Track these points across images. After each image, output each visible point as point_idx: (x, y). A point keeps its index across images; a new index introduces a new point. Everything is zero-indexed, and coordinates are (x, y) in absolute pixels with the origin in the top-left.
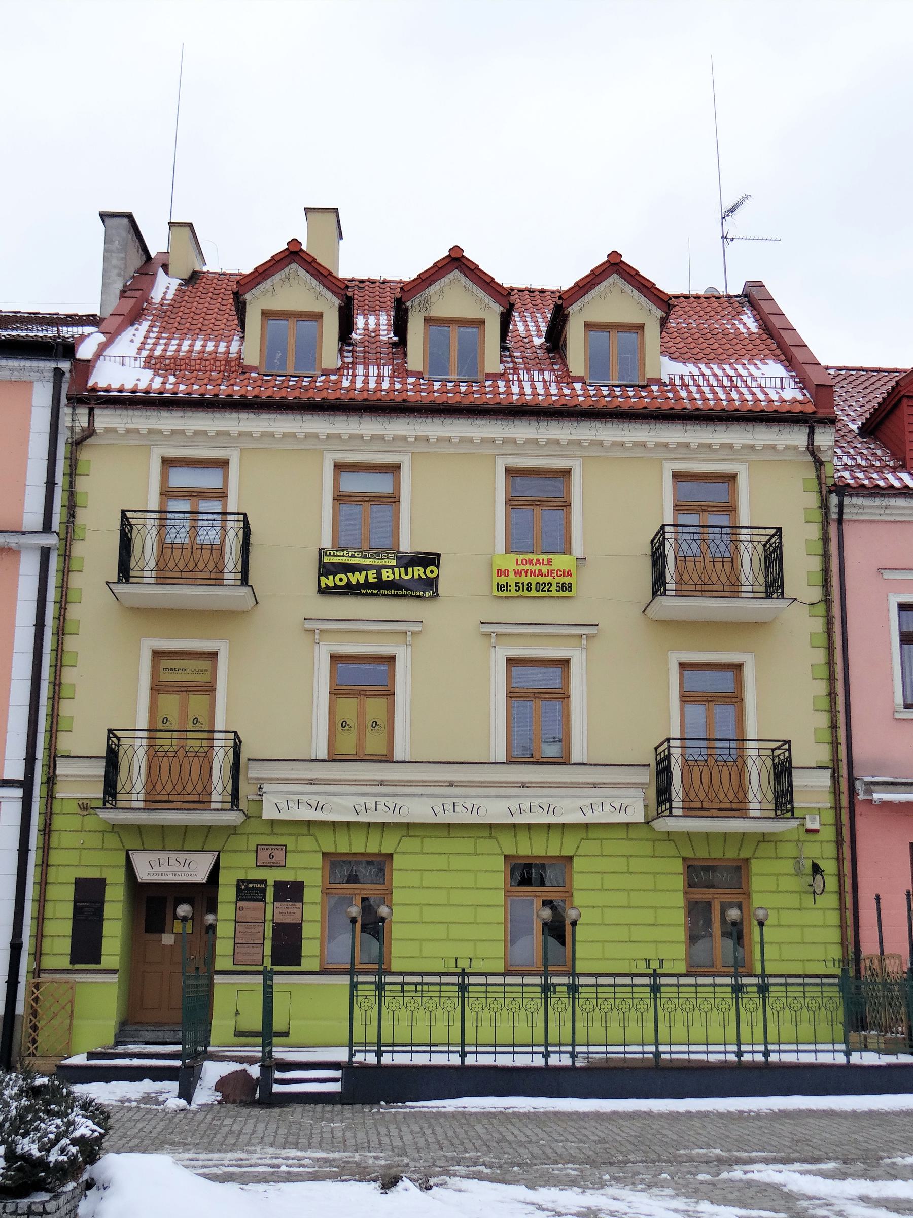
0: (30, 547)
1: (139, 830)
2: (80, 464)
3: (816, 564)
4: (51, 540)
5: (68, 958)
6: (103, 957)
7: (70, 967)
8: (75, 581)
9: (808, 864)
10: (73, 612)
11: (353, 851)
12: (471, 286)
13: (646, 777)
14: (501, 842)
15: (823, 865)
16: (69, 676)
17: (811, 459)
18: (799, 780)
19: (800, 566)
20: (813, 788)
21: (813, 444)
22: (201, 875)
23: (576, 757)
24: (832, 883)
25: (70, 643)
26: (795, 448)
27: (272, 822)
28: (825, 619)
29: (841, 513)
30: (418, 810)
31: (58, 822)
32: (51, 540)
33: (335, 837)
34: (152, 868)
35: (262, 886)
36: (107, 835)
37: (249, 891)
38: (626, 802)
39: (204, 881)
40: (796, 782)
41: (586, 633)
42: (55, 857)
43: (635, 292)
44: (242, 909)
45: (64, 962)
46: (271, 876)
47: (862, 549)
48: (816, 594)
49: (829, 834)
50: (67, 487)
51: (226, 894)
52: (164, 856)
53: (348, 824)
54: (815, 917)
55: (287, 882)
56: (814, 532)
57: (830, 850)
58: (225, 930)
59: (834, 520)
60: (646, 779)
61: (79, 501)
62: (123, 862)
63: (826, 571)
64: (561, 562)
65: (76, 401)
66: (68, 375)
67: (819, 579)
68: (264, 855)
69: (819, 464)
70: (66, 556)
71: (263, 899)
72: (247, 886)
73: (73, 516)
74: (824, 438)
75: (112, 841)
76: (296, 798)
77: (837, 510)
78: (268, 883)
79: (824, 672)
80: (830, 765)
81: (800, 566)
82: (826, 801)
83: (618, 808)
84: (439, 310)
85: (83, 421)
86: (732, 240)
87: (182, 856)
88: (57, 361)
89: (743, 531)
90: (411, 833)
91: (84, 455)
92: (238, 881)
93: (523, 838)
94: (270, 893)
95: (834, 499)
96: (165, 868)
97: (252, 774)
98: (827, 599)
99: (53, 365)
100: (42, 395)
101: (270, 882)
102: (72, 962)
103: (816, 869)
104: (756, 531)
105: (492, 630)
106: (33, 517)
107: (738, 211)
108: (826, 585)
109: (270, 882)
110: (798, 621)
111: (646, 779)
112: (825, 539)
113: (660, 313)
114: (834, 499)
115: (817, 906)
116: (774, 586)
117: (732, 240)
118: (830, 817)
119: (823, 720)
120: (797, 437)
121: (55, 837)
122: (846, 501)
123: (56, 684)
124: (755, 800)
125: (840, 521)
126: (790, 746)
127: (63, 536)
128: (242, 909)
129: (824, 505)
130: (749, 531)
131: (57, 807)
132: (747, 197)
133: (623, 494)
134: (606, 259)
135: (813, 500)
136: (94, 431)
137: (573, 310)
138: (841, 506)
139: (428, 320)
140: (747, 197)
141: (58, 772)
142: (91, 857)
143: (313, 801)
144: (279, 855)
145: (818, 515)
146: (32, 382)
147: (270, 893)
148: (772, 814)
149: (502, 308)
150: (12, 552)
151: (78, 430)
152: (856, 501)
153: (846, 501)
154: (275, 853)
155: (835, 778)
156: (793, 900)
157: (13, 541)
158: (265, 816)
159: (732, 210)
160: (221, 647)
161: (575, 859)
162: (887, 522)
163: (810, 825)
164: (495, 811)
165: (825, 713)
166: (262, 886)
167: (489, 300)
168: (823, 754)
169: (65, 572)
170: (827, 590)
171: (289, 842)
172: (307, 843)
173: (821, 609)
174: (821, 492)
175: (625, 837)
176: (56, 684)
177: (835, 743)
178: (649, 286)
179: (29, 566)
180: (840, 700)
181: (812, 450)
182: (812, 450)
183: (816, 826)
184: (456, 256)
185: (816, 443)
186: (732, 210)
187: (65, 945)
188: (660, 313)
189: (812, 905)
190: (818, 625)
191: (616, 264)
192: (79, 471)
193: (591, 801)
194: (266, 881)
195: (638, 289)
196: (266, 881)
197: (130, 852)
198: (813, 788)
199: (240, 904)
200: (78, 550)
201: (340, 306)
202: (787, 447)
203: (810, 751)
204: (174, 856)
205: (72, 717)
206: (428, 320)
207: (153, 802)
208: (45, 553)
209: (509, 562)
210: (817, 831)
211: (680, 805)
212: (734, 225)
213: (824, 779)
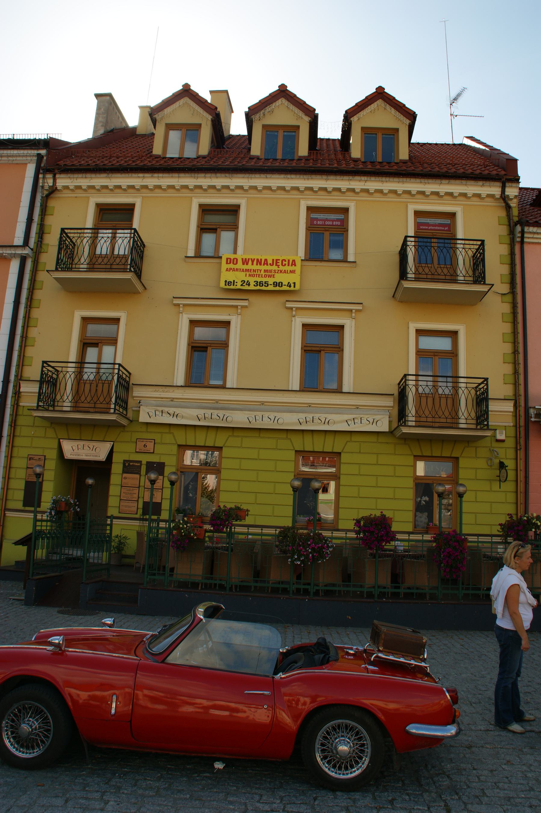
0: (14, 256)
2: (48, 209)
3: (505, 270)
4: (26, 251)
5: (21, 503)
6: (42, 503)
7: (23, 508)
9: (497, 461)
11: (188, 444)
12: (292, 107)
13: (389, 402)
15: (506, 462)
16: (33, 332)
17: (504, 204)
18: (493, 406)
20: (501, 411)
21: (504, 194)
22: (102, 456)
24: (511, 475)
25: (35, 313)
26: (492, 196)
27: (147, 424)
28: (512, 305)
29: (522, 237)
30: (239, 419)
31: (21, 421)
32: (26, 251)
33: (186, 434)
34: (73, 450)
35: (139, 464)
36: (48, 429)
37: (130, 467)
38: (377, 417)
39: (104, 460)
40: (491, 408)
42: (18, 442)
43: (393, 109)
44: (125, 478)
45: (19, 505)
46: (145, 459)
48: (505, 288)
49: (511, 443)
50: (40, 222)
51: (117, 468)
52: (81, 443)
53: (195, 426)
55: (154, 463)
56: (504, 250)
57: (511, 453)
58: (114, 490)
59: (518, 242)
60: (391, 404)
61: (46, 230)
62: (56, 446)
63: (513, 274)
66: (45, 158)
67: (507, 279)
68: (140, 445)
71: (139, 473)
72: (129, 464)
73: (42, 238)
76: (161, 409)
77: (519, 235)
78: (143, 463)
79: (510, 338)
80: (513, 398)
82: (510, 422)
83: (371, 422)
85: (50, 182)
86: (456, 116)
87: (91, 444)
88: (38, 149)
89: (459, 242)
90: (235, 434)
91: (51, 203)
92: (124, 460)
93: (308, 438)
94: (143, 469)
96: (81, 451)
97: (135, 394)
98: (513, 292)
99: (36, 152)
100: (31, 169)
101: (144, 462)
102: (25, 505)
103: (502, 465)
104: (467, 242)
106: (19, 240)
107: (460, 100)
109: (144, 462)
111: (391, 404)
112: (512, 254)
113: (408, 122)
114: (519, 228)
115: (502, 489)
117: (456, 116)
118: (512, 432)
121: (18, 429)
122: (526, 229)
123: (24, 337)
124: (463, 417)
125: (522, 242)
126: (487, 382)
127: (35, 250)
128: (125, 478)
129: (512, 232)
130: (463, 242)
131: (20, 411)
132: (464, 89)
134: (375, 91)
135: (504, 230)
136: (56, 188)
137: (354, 119)
138: (523, 232)
140: (464, 89)
141: (21, 390)
143: (171, 410)
144: (150, 446)
145: (507, 240)
146: (27, 164)
147: (143, 469)
148: (474, 426)
149: (310, 119)
150: (7, 259)
151: (46, 188)
152: (531, 229)
153: (526, 229)
154: (148, 444)
155: (516, 406)
158: (141, 419)
159: (455, 99)
160: (123, 315)
161: (342, 454)
163: (499, 437)
164: (289, 420)
165: (511, 364)
166: (139, 464)
167: (301, 114)
168: (508, 390)
170: (513, 285)
171: (157, 437)
172: (168, 438)
173: (509, 298)
174: (510, 225)
175: (376, 441)
176: (24, 337)
177: (516, 384)
178: (402, 106)
179: (14, 266)
181: (504, 198)
183: (503, 437)
184: (283, 89)
185: (506, 193)
186: (455, 99)
187: (20, 495)
188: (408, 122)
189: (499, 489)
190: (507, 308)
191: (381, 93)
192: (47, 213)
193: (354, 416)
194: (141, 461)
195: (395, 108)
196: (141, 461)
197: (61, 440)
198: (501, 411)
199: (125, 475)
201: (212, 121)
202: (489, 196)
203: (500, 388)
204: (86, 443)
205: (32, 357)
207: (76, 408)
208: (23, 260)
210: (503, 441)
211: (414, 419)
212: (458, 108)
213: (509, 407)
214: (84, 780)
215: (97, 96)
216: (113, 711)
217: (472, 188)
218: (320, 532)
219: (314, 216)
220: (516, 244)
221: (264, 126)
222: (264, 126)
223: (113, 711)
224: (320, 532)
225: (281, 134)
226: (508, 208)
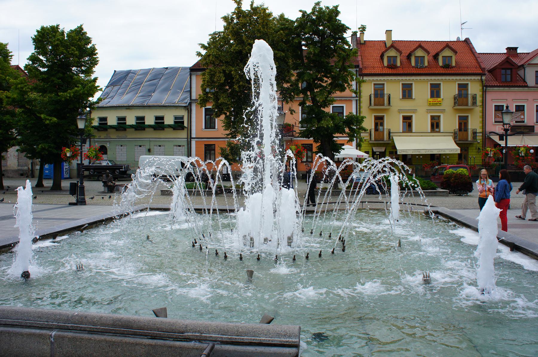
1: (374, 143)
3: (481, 99)
4: (358, 99)
8: (361, 105)
10: (362, 110)
14: (474, 62)
19: (479, 99)
23: (442, 130)
41: (443, 111)
47: (489, 96)
48: (481, 104)
49: (481, 143)
54: (478, 156)
56: (481, 93)
57: (481, 145)
64: (439, 99)
65: (360, 75)
69: (482, 82)
70: (360, 100)
74: (484, 78)
75: (370, 145)
81: (479, 99)
84: (417, 55)
95: (485, 88)
103: (479, 149)
105: (428, 111)
108: (483, 102)
110: (478, 109)
112: (483, 94)
114: (485, 88)
116: (474, 103)
118: (481, 140)
119: (481, 125)
120: (479, 78)
129: (483, 89)
133: (449, 89)
135: (481, 88)
139: (415, 57)
142: (366, 148)
156: (475, 153)
157: (352, 99)
162: (22, 326)
168: (481, 130)
169: (360, 103)
177: (483, 128)
180: (343, 99)
181: (481, 79)
182: (481, 79)
190: (481, 109)
200: (361, 99)
203: (479, 130)
206: (415, 57)
208: (357, 100)
209: (431, 100)
214: (199, 267)
215: (222, 18)
216: (89, 47)
217: (473, 78)
218: (66, 35)
219: (376, 86)
220: (484, 92)
221: (443, 57)
222: (443, 57)
223: (89, 47)
224: (66, 35)
225: (392, 58)
226: (482, 82)
